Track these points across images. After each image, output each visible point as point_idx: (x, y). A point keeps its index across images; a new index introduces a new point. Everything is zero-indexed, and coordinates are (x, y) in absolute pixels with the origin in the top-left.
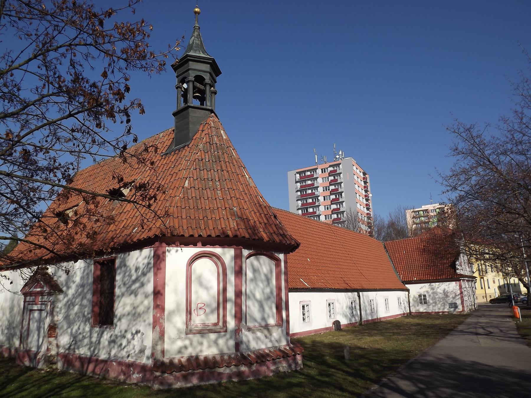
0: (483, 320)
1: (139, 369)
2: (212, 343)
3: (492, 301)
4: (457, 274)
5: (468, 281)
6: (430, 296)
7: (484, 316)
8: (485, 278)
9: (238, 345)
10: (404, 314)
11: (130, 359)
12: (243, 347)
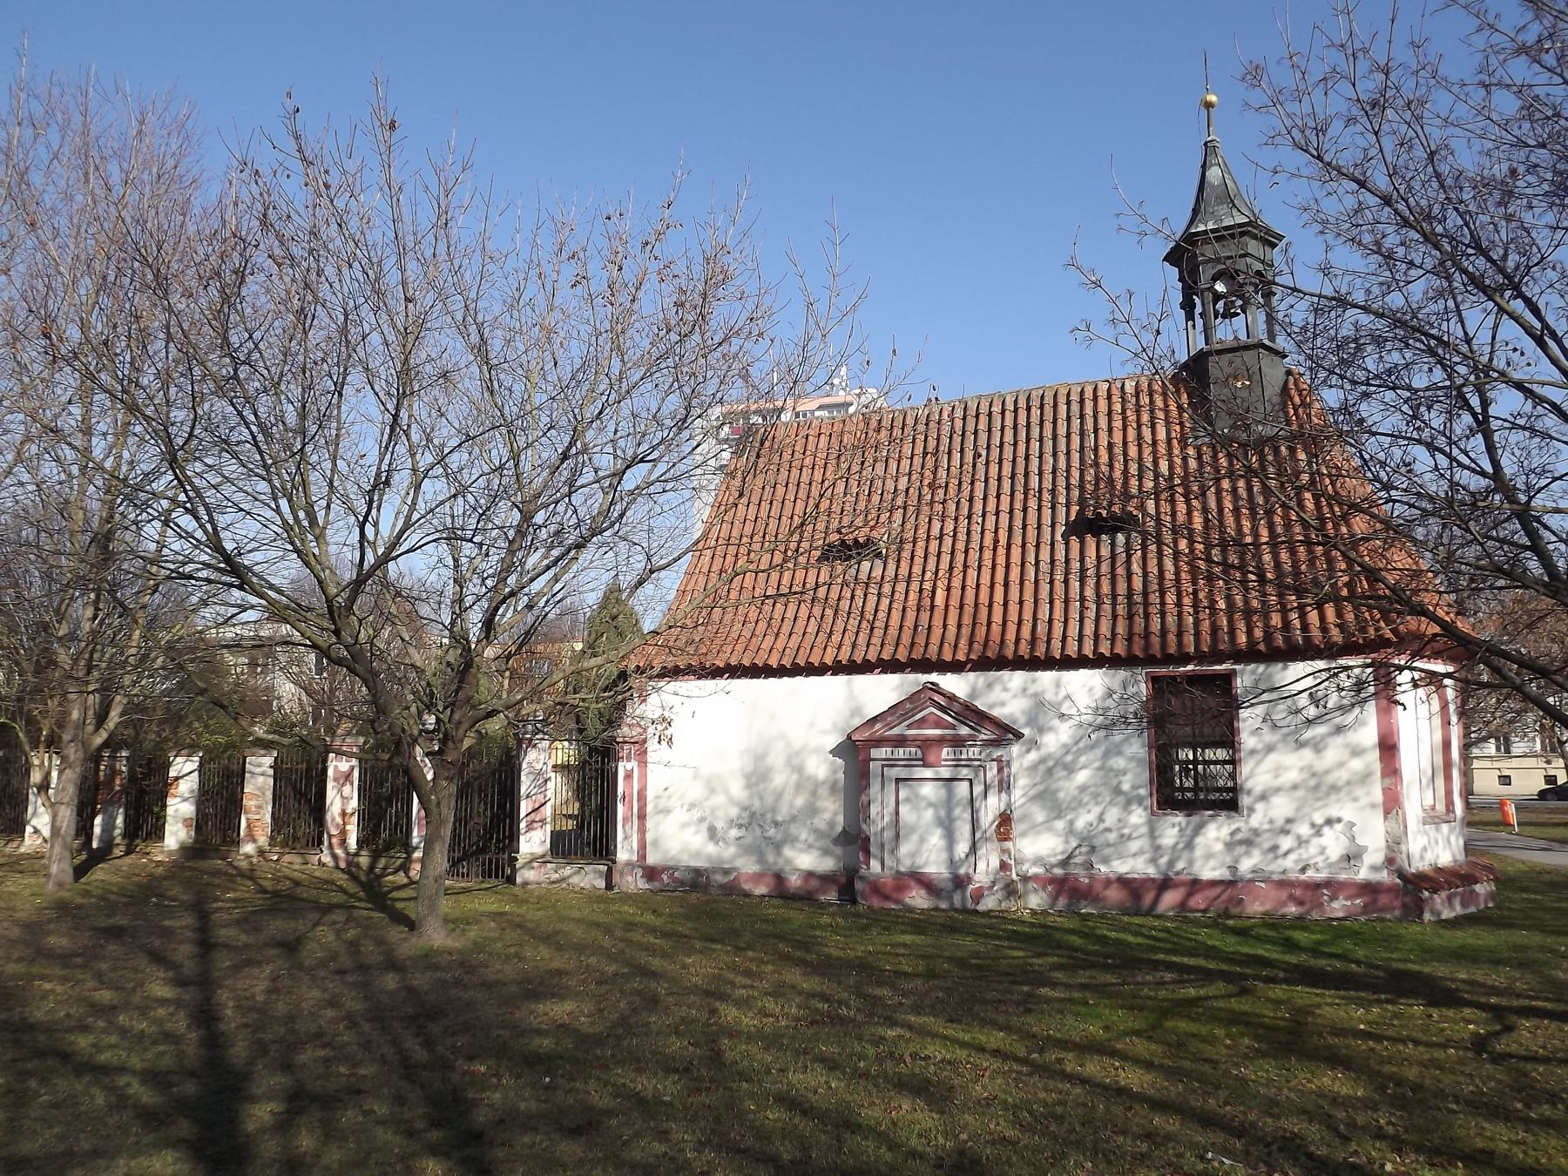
1: (1353, 891)
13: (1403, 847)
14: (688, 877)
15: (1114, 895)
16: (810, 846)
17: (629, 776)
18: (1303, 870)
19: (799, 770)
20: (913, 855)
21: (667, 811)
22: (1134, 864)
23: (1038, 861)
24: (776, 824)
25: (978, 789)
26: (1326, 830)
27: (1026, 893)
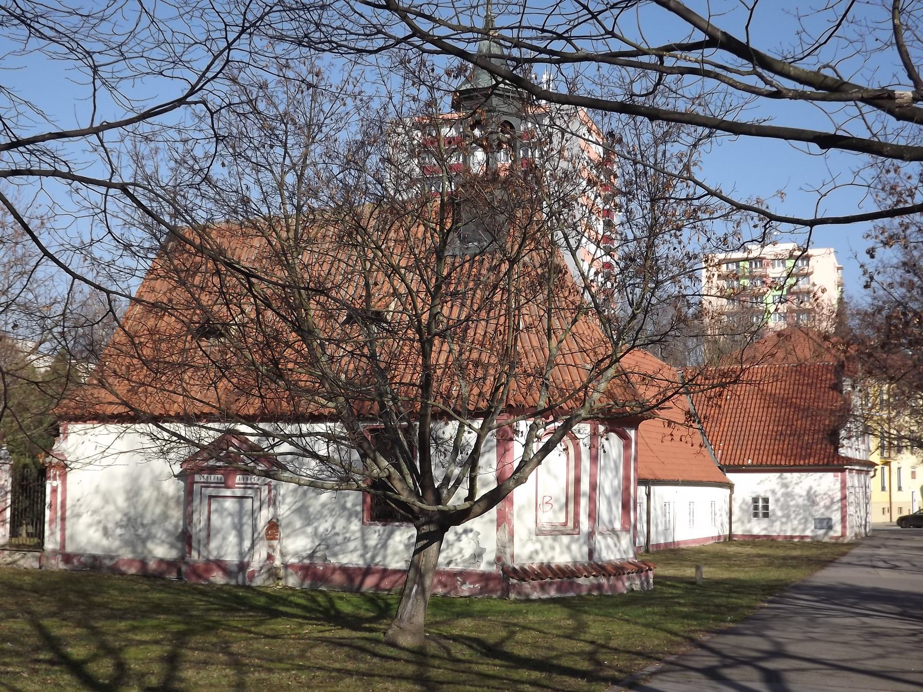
0: (883, 552)
1: (476, 578)
2: (565, 549)
3: (903, 521)
4: (840, 458)
5: (859, 472)
6: (777, 500)
7: (886, 546)
8: (894, 465)
9: (591, 553)
10: (719, 537)
11: (452, 566)
12: (596, 556)
13: (508, 551)
14: (90, 561)
15: (338, 578)
16: (163, 542)
17: (54, 490)
18: (449, 563)
19: (158, 489)
20: (220, 548)
21: (79, 516)
22: (352, 559)
23: (296, 554)
24: (143, 525)
25: (257, 504)
26: (463, 536)
27: (286, 576)
